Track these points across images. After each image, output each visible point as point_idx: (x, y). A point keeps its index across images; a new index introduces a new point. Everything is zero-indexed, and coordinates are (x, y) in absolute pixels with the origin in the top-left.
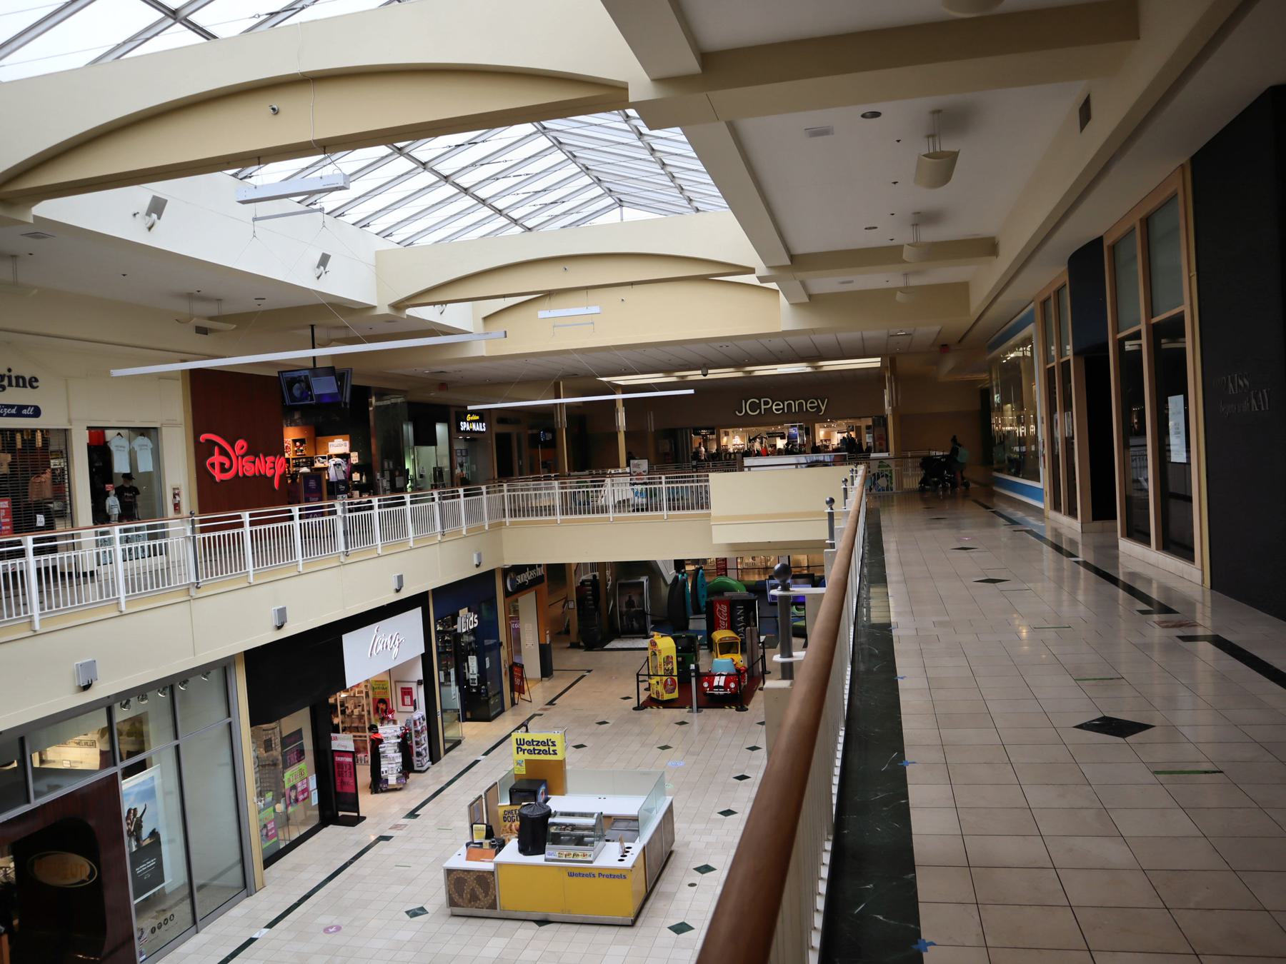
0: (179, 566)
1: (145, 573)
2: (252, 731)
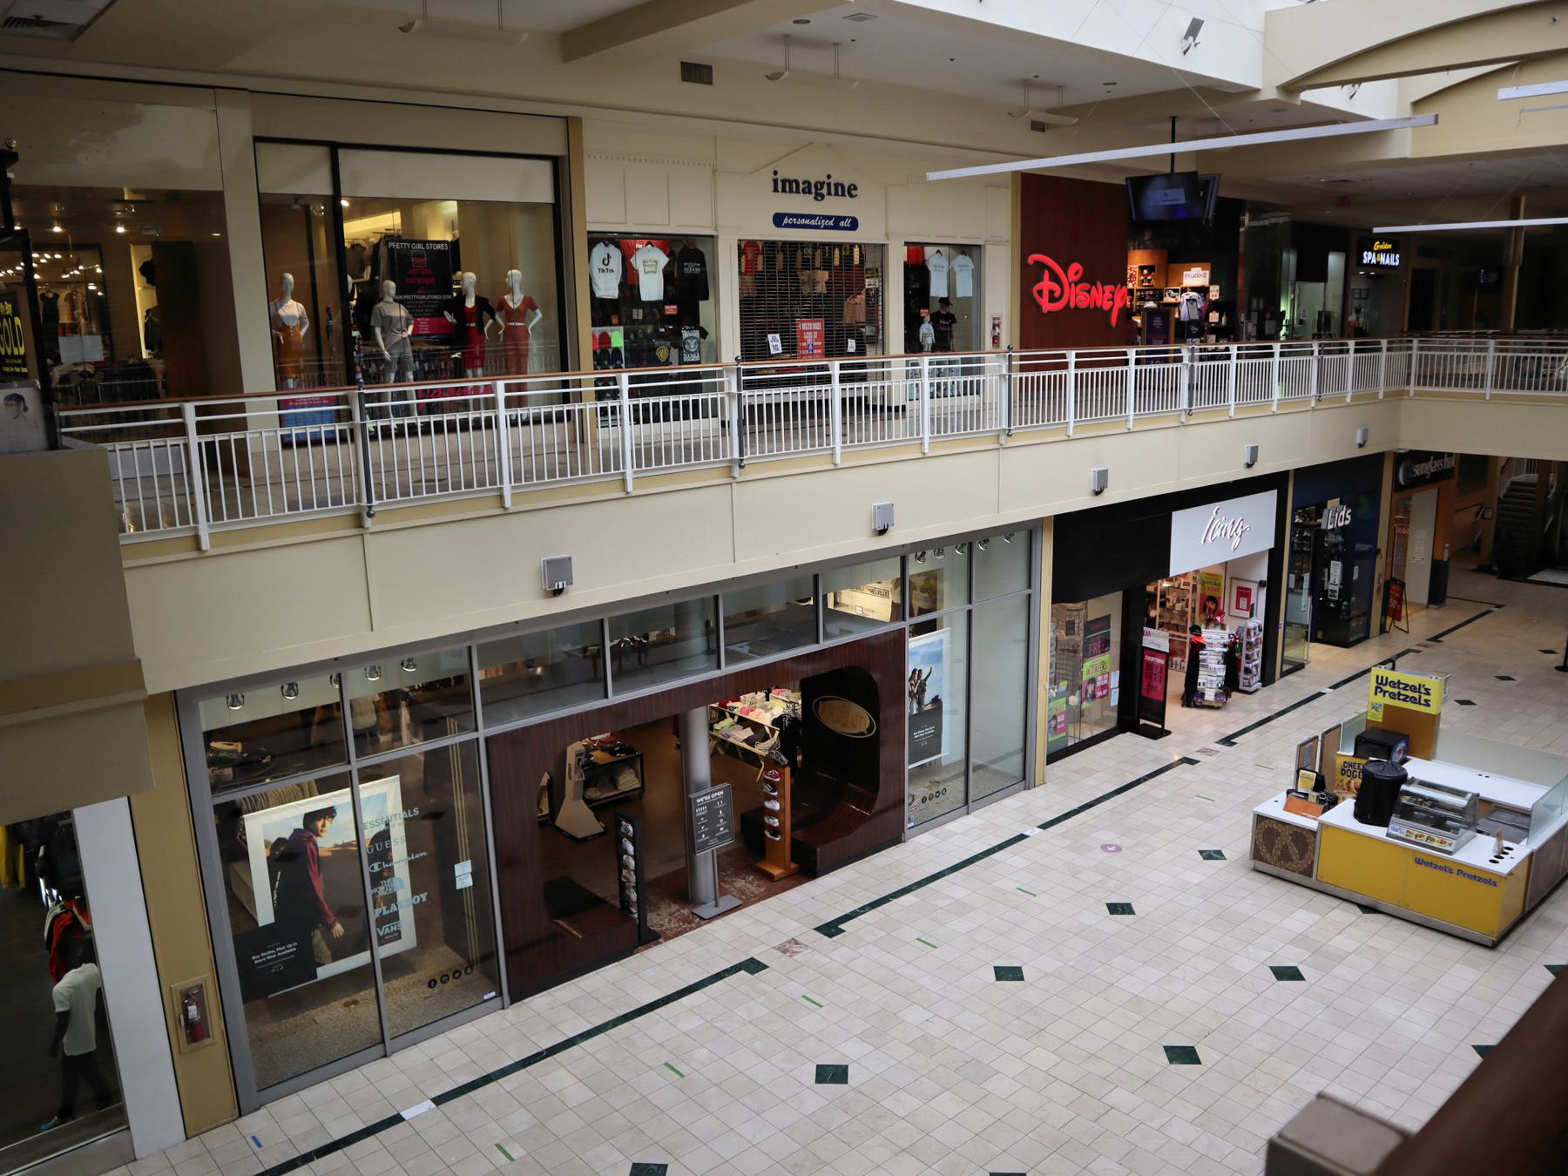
0: (991, 409)
1: (952, 413)
2: (1052, 609)
